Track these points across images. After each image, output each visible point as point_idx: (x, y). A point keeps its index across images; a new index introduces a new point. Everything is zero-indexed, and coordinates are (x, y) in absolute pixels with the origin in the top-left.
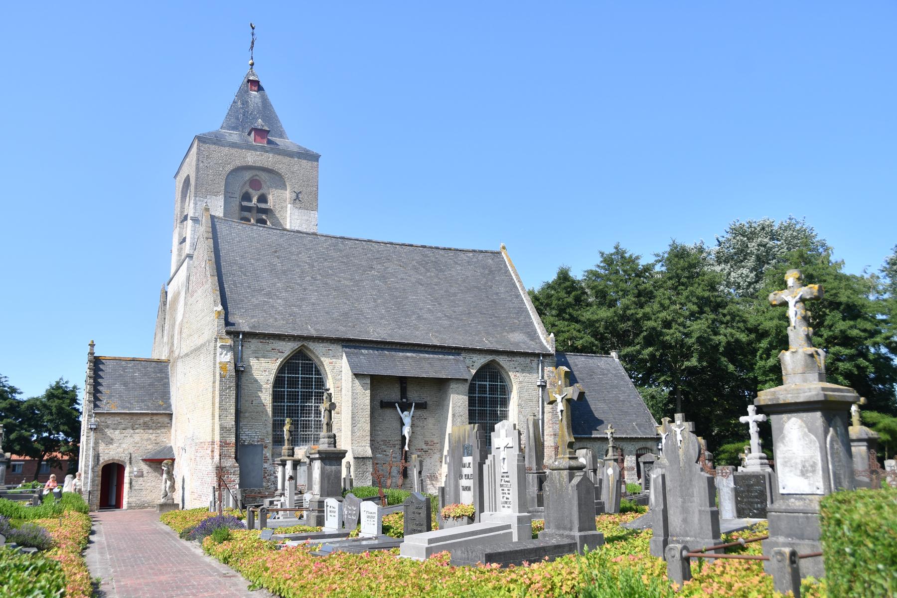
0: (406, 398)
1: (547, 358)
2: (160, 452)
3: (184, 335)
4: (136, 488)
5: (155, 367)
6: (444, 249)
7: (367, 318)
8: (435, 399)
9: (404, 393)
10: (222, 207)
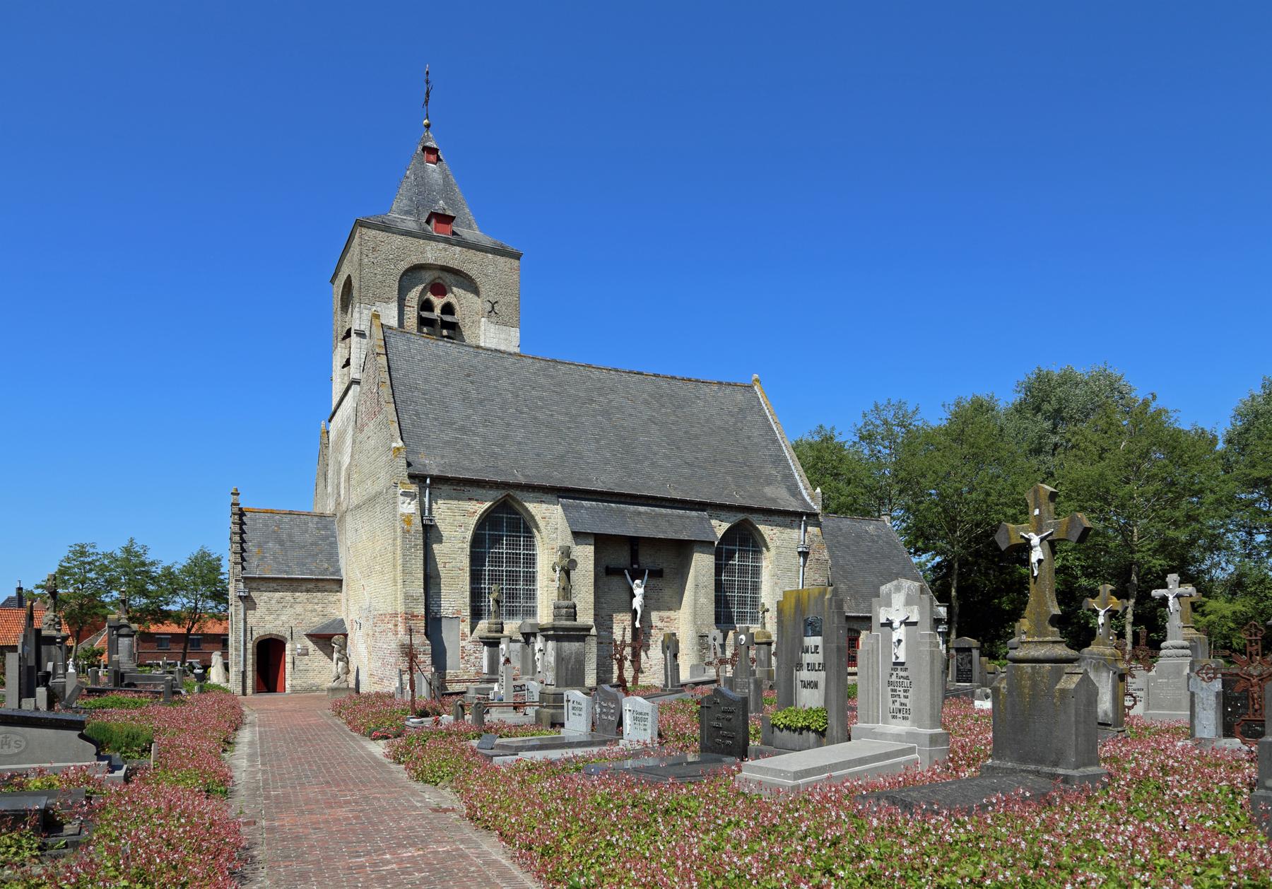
0: (637, 563)
2: (328, 626)
3: (353, 482)
4: (301, 668)
5: (317, 523)
6: (683, 379)
7: (589, 463)
9: (634, 557)
10: (396, 319)
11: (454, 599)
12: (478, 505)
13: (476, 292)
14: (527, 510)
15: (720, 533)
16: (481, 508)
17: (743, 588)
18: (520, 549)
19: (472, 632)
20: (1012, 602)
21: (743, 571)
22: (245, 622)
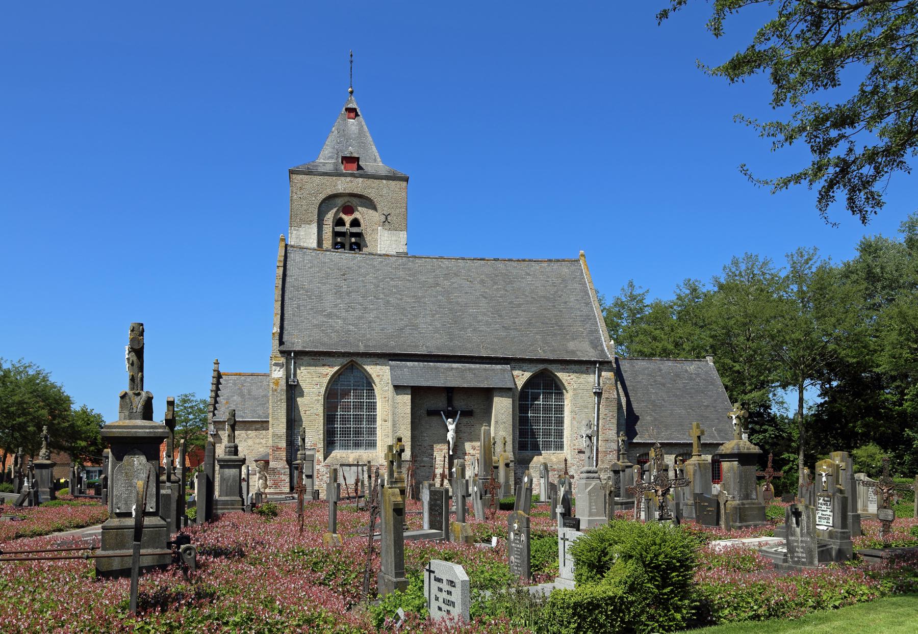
9: (450, 402)
11: (314, 434)
12: (330, 369)
13: (375, 208)
14: (365, 370)
15: (520, 383)
16: (331, 371)
17: (547, 421)
18: (363, 399)
19: (325, 459)
20: (865, 425)
21: (547, 409)
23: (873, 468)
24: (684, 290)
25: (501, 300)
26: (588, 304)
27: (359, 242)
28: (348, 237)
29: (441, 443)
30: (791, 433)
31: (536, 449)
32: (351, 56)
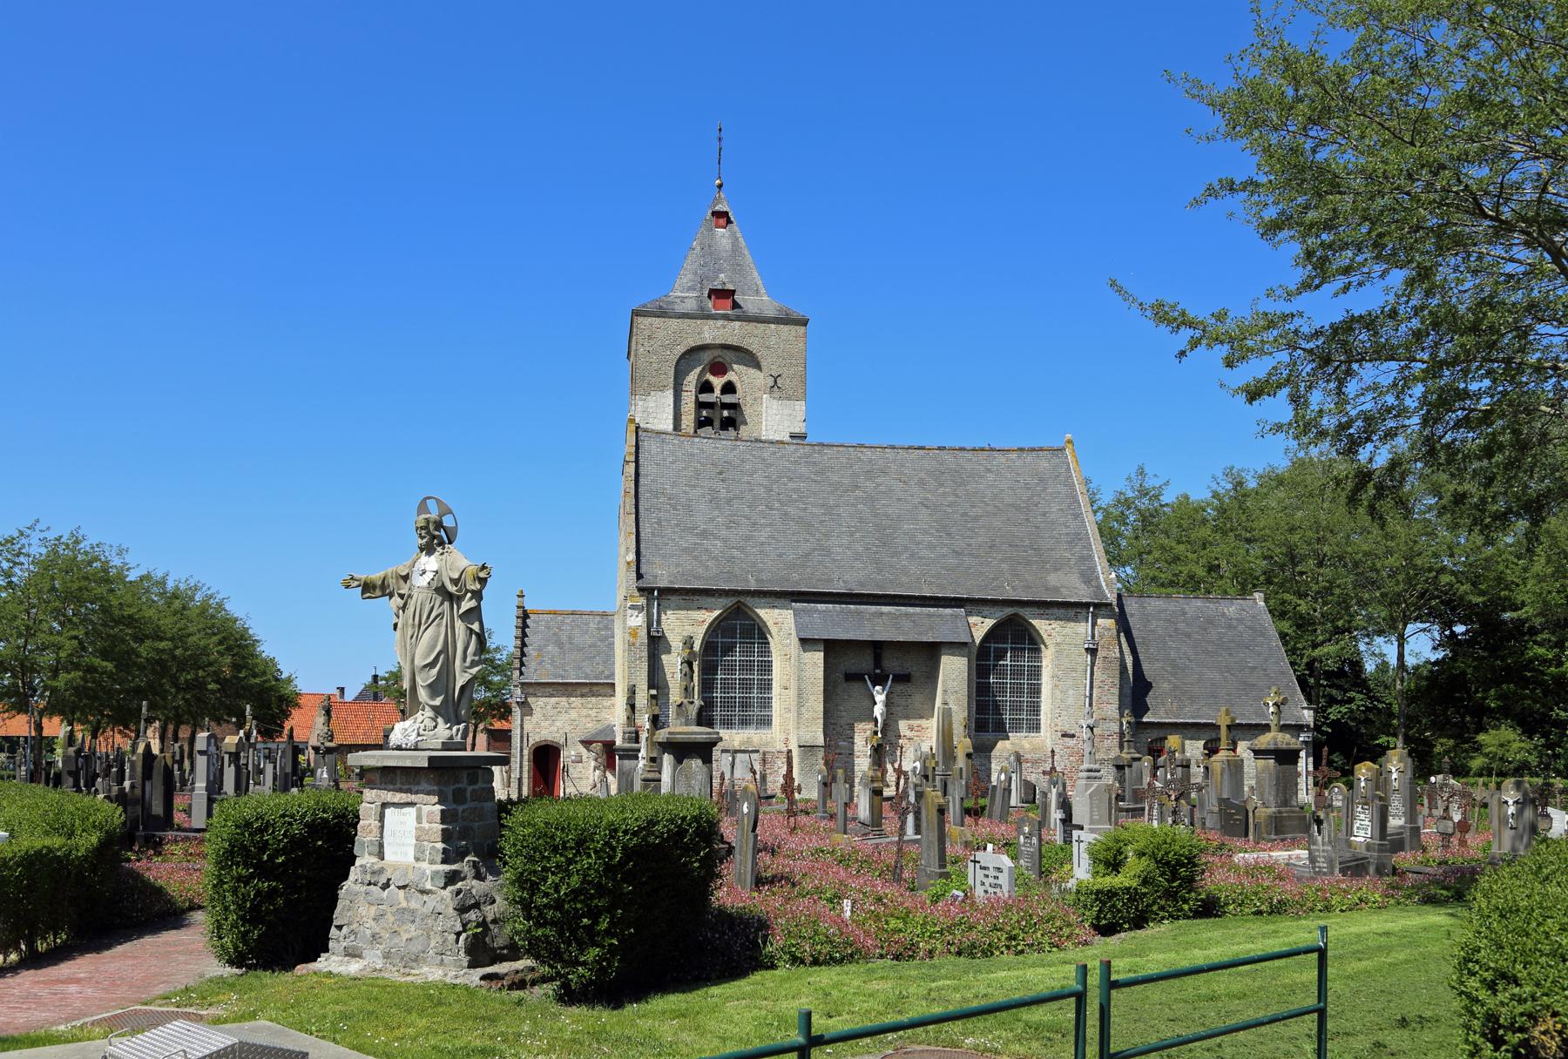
1: (1103, 608)
2: (601, 731)
5: (599, 622)
6: (974, 450)
8: (924, 669)
9: (878, 662)
13: (758, 366)
15: (979, 635)
16: (709, 616)
17: (1017, 690)
21: (1017, 672)
22: (522, 728)
23: (1510, 763)
24: (1223, 483)
25: (949, 510)
26: (1078, 516)
27: (733, 416)
28: (717, 409)
29: (865, 721)
30: (1391, 704)
31: (1001, 730)
32: (720, 130)
